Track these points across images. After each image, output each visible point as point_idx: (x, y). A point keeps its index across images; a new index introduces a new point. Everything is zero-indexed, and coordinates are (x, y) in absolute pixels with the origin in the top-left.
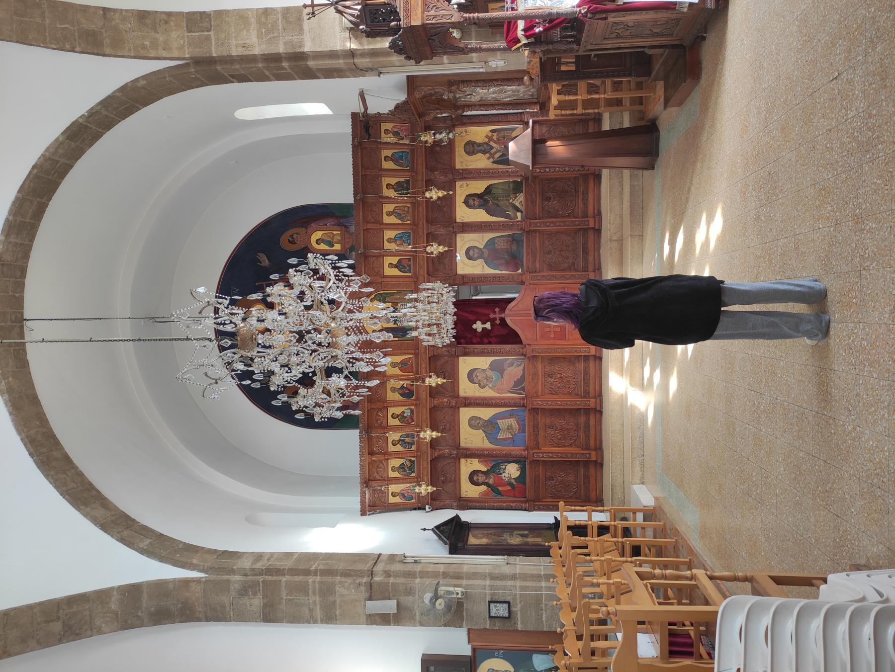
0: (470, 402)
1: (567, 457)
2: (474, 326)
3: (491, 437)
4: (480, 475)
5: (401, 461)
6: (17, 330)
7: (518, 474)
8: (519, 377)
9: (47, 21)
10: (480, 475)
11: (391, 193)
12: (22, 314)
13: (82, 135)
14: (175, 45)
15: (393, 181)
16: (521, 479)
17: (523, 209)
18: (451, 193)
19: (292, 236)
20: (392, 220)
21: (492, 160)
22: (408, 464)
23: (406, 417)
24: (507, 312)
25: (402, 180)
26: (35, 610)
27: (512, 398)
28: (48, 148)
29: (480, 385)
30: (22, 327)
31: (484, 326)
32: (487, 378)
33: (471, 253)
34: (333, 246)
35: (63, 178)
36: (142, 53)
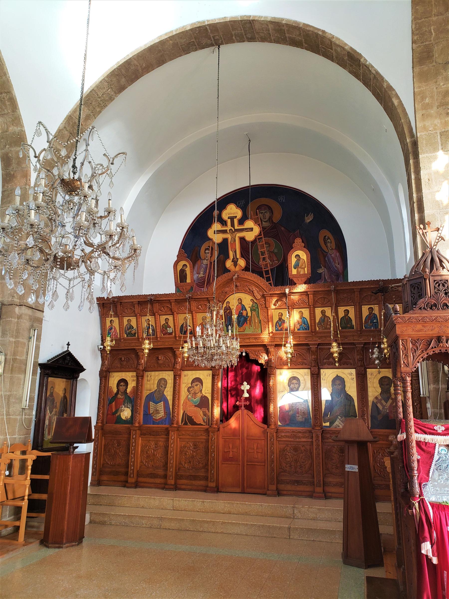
0: (177, 378)
1: (132, 458)
2: (245, 383)
3: (151, 397)
4: (124, 387)
5: (135, 327)
6: (209, 42)
7: (123, 417)
8: (195, 420)
9: (434, 19)
10: (124, 387)
11: (341, 314)
12: (222, 44)
13: (351, 62)
14: (428, 123)
15: (352, 315)
16: (119, 420)
17: (333, 428)
18: (337, 365)
19: (329, 238)
20: (318, 315)
21: (375, 401)
22: (133, 332)
23: (166, 329)
24: (246, 411)
25: (354, 323)
26: (4, 77)
27: (178, 414)
28: (339, 39)
29: (190, 387)
30: (212, 45)
31: (245, 392)
32: (195, 394)
33: (294, 381)
34: (295, 268)
35: (323, 56)
36: (418, 97)
